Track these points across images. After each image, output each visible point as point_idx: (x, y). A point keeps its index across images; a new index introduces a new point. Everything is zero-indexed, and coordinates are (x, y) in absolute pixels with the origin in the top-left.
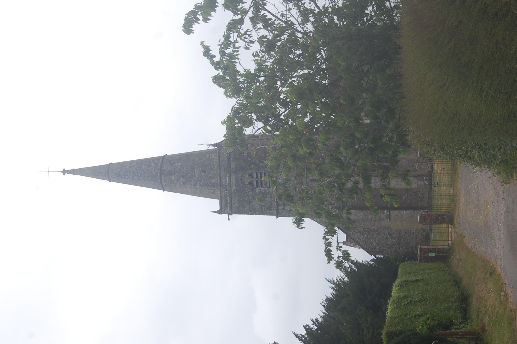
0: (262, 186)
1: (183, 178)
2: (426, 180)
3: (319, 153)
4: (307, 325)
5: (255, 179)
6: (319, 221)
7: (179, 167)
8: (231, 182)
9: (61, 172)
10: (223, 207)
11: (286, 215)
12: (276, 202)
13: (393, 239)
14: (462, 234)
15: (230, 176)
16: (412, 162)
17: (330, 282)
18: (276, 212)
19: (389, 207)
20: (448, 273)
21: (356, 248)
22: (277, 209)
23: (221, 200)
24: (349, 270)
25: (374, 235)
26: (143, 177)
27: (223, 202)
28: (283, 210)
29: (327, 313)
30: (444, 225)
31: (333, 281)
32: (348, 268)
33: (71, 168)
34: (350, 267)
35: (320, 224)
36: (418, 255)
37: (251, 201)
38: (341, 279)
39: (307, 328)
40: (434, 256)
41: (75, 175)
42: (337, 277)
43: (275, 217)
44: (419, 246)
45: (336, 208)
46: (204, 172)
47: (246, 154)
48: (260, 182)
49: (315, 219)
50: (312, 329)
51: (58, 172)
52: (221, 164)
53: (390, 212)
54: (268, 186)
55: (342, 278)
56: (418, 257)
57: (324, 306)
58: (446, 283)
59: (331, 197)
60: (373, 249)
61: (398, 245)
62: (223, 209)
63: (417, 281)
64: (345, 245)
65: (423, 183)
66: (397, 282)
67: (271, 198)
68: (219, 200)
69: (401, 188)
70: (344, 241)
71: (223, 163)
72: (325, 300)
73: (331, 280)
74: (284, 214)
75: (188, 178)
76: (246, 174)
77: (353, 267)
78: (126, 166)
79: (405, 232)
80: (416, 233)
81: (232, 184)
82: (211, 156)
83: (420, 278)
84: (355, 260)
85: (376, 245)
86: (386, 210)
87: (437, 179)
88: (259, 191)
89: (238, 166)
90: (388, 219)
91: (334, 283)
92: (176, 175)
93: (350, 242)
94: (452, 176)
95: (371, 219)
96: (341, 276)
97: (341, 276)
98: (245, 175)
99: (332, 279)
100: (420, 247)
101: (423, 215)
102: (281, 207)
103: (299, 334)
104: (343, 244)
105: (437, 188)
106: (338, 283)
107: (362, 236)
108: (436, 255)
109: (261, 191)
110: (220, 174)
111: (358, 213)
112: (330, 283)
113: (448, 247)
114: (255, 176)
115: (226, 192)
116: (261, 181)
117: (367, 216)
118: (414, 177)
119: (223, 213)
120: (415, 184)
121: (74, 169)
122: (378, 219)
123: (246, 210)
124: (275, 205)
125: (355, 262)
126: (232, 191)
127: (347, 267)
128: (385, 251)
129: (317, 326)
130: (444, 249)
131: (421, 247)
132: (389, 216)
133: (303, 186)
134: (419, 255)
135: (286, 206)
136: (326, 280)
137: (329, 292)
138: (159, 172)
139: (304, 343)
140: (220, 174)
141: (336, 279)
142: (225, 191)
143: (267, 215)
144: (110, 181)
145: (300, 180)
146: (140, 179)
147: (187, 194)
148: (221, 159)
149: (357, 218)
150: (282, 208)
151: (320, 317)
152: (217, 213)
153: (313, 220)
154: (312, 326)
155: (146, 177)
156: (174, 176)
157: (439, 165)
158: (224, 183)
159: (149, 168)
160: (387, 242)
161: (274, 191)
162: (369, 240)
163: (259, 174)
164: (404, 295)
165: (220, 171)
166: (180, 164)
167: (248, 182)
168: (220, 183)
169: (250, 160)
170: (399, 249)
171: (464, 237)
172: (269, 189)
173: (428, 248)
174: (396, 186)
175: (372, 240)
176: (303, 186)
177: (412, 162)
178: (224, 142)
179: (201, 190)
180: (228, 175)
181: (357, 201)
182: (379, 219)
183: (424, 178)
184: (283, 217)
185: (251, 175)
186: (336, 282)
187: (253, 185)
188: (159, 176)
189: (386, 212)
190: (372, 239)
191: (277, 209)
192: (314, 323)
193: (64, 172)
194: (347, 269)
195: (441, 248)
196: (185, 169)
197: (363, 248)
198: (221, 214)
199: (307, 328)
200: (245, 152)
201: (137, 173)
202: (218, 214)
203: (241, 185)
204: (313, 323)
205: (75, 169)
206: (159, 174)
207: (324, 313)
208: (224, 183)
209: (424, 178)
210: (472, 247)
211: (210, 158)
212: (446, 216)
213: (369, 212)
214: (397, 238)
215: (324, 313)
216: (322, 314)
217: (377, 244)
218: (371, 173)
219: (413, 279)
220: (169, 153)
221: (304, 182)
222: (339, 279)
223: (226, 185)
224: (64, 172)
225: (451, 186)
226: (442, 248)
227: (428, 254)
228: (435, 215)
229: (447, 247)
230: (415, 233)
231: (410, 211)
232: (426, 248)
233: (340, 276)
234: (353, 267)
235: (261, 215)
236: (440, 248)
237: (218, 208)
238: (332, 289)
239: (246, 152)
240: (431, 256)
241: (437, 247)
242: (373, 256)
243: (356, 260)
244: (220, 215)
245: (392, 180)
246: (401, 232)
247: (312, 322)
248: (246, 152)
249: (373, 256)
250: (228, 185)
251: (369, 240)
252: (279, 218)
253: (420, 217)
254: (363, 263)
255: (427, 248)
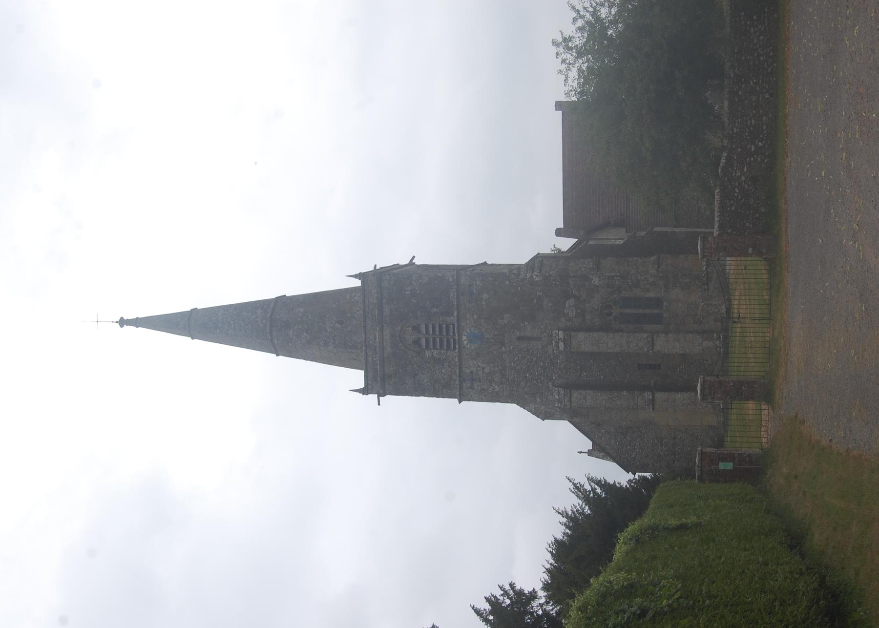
0: (434, 347)
1: (306, 333)
2: (719, 338)
3: (531, 291)
4: (493, 596)
5: (424, 335)
6: (533, 410)
7: (300, 315)
8: (383, 339)
9: (117, 322)
10: (369, 382)
11: (475, 398)
12: (458, 375)
13: (664, 447)
14: (796, 416)
15: (381, 330)
16: (694, 308)
17: (561, 514)
18: (458, 393)
19: (653, 386)
20: (763, 509)
21: (607, 460)
22: (460, 387)
23: (367, 371)
24: (592, 495)
25: (632, 438)
26: (243, 332)
27: (370, 374)
28: (470, 390)
29: (555, 564)
30: (751, 405)
31: (567, 513)
32: (590, 492)
33: (133, 317)
34: (594, 490)
35: (536, 416)
36: (696, 467)
37: (416, 372)
38: (580, 509)
39: (493, 602)
40: (730, 470)
41: (140, 328)
42: (573, 507)
43: (456, 400)
44: (699, 449)
45: (559, 386)
46: (341, 323)
47: (409, 292)
48: (431, 339)
49: (526, 407)
50: (503, 603)
51: (113, 322)
52: (367, 309)
53: (653, 397)
54: (445, 348)
55: (580, 507)
56: (697, 471)
57: (551, 553)
58: (763, 537)
59: (552, 367)
60: (630, 462)
61: (673, 456)
62: (370, 387)
63: (682, 527)
64: (590, 456)
65: (712, 344)
66: (633, 528)
67: (450, 369)
68: (363, 371)
69: (674, 353)
70: (589, 450)
71: (371, 307)
72: (552, 543)
73: (562, 511)
74: (472, 396)
75: (314, 334)
76: (409, 327)
77: (599, 490)
78: (217, 313)
79: (684, 434)
80: (702, 437)
81: (385, 343)
82: (354, 296)
83: (692, 519)
84: (602, 479)
85: (636, 456)
86: (646, 392)
87: (738, 334)
88: (430, 356)
89: (396, 313)
90: (651, 406)
91: (567, 516)
92: (296, 327)
93: (598, 452)
94: (770, 300)
95: (620, 407)
96: (579, 504)
97: (579, 504)
98: (407, 327)
99: (564, 510)
100: (701, 451)
101: (708, 383)
102: (466, 384)
103: (483, 609)
104: (587, 454)
105: (739, 325)
106: (573, 516)
107: (613, 441)
108: (734, 468)
109: (433, 355)
110: (365, 327)
111: (598, 396)
112: (561, 516)
113: (761, 451)
114: (424, 330)
115: (375, 357)
116: (440, 340)
117: (614, 401)
118: (697, 333)
119: (370, 394)
120: (699, 346)
121: (137, 318)
122: (633, 407)
123: (407, 387)
124: (456, 380)
125: (603, 483)
126: (385, 355)
127: (588, 490)
128: (650, 466)
129: (510, 599)
130: (751, 454)
131: (704, 451)
132: (653, 401)
133: (504, 349)
134: (698, 467)
135: (474, 382)
136: (555, 511)
137: (558, 530)
138: (268, 323)
139: (490, 626)
140: (365, 327)
141: (571, 510)
142: (374, 356)
143: (443, 398)
144: (193, 339)
145: (499, 337)
146: (239, 334)
147: (315, 361)
148: (367, 301)
149: (596, 405)
150: (469, 385)
151: (545, 570)
152: (360, 393)
153: (524, 409)
154: (501, 598)
155: (247, 331)
156: (292, 330)
157: (742, 302)
158: (371, 342)
159: (253, 317)
160: (655, 451)
161: (456, 356)
162: (624, 448)
163: (430, 326)
164: (625, 584)
165: (365, 321)
166: (302, 310)
167: (411, 341)
168: (365, 341)
169: (415, 301)
170: (674, 462)
171: (803, 422)
172: (447, 353)
173: (719, 452)
174: (664, 350)
175: (629, 447)
176: (504, 349)
177: (694, 308)
178: (372, 273)
179: (337, 355)
180: (378, 329)
181: (598, 375)
182: (634, 407)
183: (715, 335)
184: (470, 401)
185: (416, 328)
186: (571, 515)
187: (420, 346)
188: (268, 329)
189: (648, 395)
190: (630, 445)
191: (461, 387)
192: (505, 593)
193: (122, 322)
194: (588, 493)
195: (745, 453)
196: (310, 317)
197: (614, 460)
198: (367, 395)
199: (493, 602)
200: (407, 289)
201: (233, 324)
202: (361, 394)
203: (400, 344)
204: (502, 592)
205: (140, 317)
206: (268, 326)
207: (551, 564)
208: (371, 342)
209: (715, 335)
210: (834, 441)
211: (352, 300)
212: (756, 386)
213: (618, 394)
214: (670, 445)
215: (551, 564)
216: (548, 566)
217: (637, 453)
218: (622, 326)
219: (674, 522)
220: (289, 293)
221: (506, 341)
222: (575, 510)
223: (376, 345)
224: (122, 322)
225: (768, 321)
226: (747, 453)
227: (719, 465)
228: (732, 381)
229: (757, 450)
230: (699, 437)
231: (689, 393)
232: (713, 453)
233: (577, 505)
234: (599, 490)
235: (433, 397)
236: (743, 452)
237: (361, 385)
238: (563, 526)
239: (409, 289)
240: (723, 470)
241: (737, 450)
242: (630, 473)
243: (604, 480)
244: (365, 395)
245: (658, 339)
246: (678, 435)
247: (502, 590)
248: (409, 289)
249: (630, 473)
250: (378, 345)
251: (624, 448)
252: (463, 402)
253: (701, 385)
254: (616, 485)
255: (715, 453)
